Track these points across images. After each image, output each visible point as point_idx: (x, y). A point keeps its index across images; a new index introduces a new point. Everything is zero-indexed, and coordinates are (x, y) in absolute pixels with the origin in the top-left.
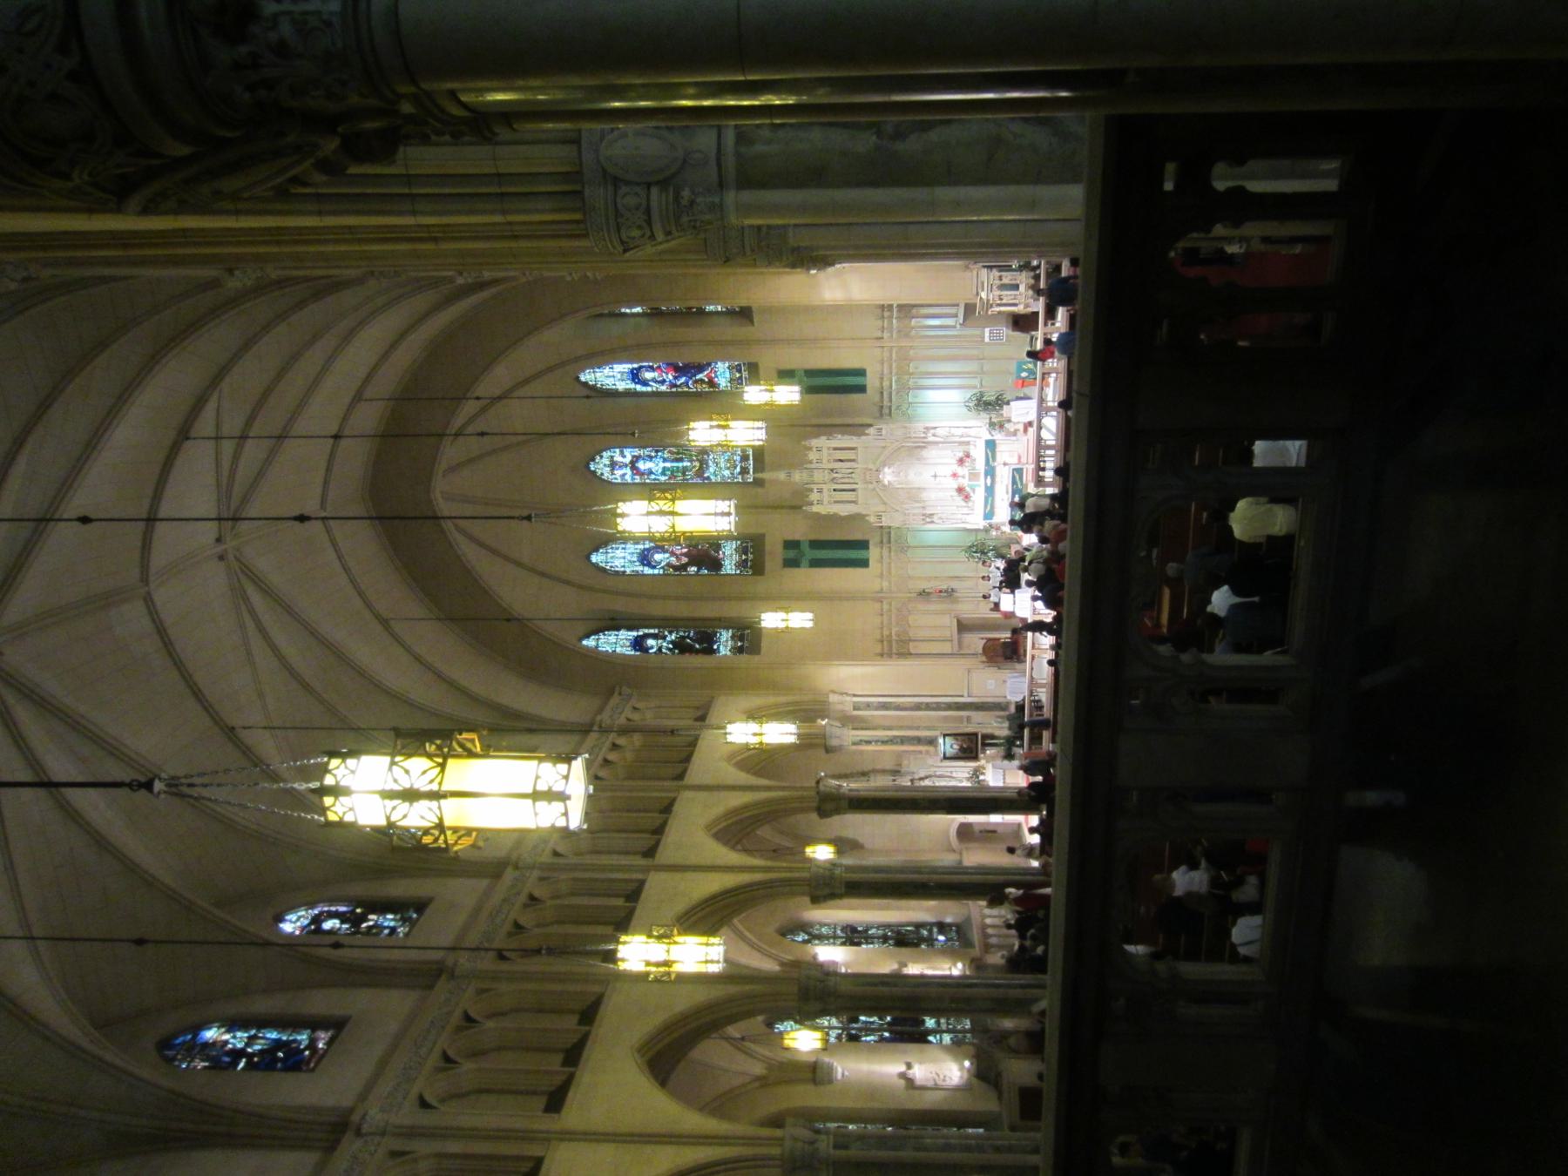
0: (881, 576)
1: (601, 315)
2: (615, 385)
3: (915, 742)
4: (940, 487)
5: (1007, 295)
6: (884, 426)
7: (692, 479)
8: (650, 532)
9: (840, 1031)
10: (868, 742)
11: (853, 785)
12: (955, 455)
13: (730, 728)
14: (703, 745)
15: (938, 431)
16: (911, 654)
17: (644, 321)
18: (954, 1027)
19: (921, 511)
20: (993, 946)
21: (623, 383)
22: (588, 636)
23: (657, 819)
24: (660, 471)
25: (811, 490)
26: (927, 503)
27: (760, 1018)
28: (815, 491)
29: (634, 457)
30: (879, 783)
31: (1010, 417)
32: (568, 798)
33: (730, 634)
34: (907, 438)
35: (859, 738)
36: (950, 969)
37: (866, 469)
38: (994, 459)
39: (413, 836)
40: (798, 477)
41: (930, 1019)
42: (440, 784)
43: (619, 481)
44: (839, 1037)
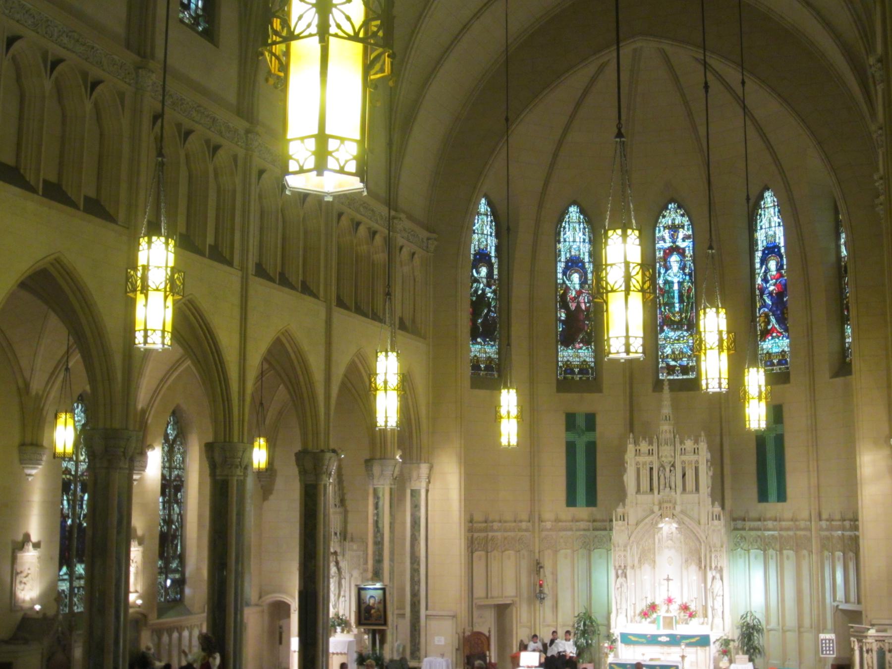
0: (557, 520)
1: (837, 212)
2: (761, 228)
3: (377, 558)
4: (657, 584)
5: (872, 658)
6: (722, 521)
7: (661, 312)
8: (606, 265)
9: (73, 473)
10: (376, 506)
11: (331, 490)
12: (692, 601)
13: (393, 356)
14: (372, 327)
15: (718, 583)
16: (472, 553)
17: (832, 258)
18: (76, 594)
19: (629, 563)
20: (160, 638)
21: (763, 238)
22: (489, 204)
23: (296, 277)
24: (669, 279)
25: (651, 443)
26: (638, 571)
27: (88, 388)
28: (650, 448)
29: (684, 250)
30: (332, 518)
31: (735, 663)
32: (320, 174)
33: (493, 356)
34: (710, 547)
35: (381, 495)
36: (136, 592)
37: (675, 503)
38: (688, 645)
39: (282, 8)
40: (666, 428)
41: (83, 569)
42: (336, 35)
43: (657, 235)
44: (67, 471)
